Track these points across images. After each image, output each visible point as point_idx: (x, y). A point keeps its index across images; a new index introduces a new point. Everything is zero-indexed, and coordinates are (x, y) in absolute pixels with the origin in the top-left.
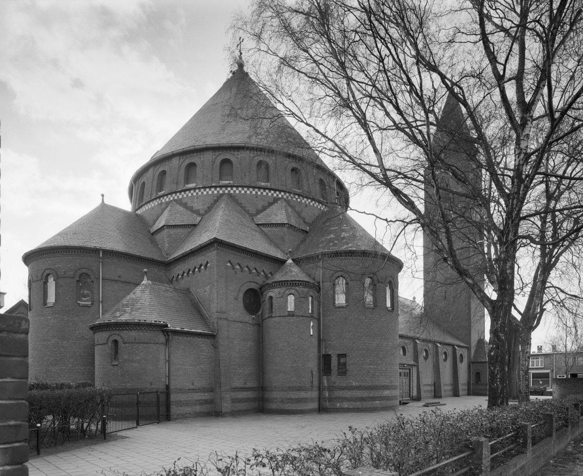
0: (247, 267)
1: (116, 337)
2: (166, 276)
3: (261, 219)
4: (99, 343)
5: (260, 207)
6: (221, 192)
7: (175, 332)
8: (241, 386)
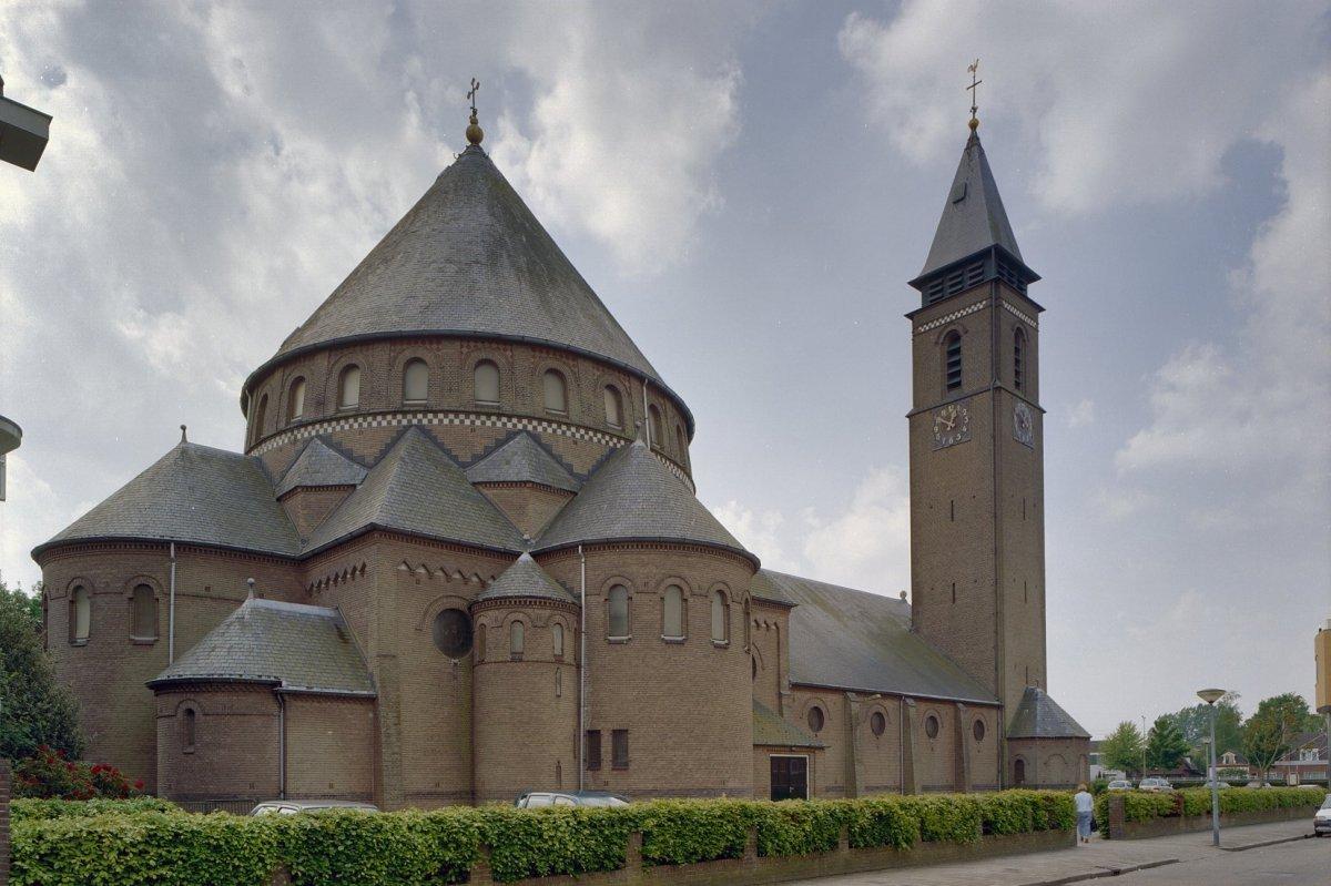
0: (442, 569)
1: (191, 705)
2: (300, 582)
3: (481, 472)
4: (163, 714)
5: (479, 450)
6: (405, 422)
7: (296, 695)
8: (428, 789)
